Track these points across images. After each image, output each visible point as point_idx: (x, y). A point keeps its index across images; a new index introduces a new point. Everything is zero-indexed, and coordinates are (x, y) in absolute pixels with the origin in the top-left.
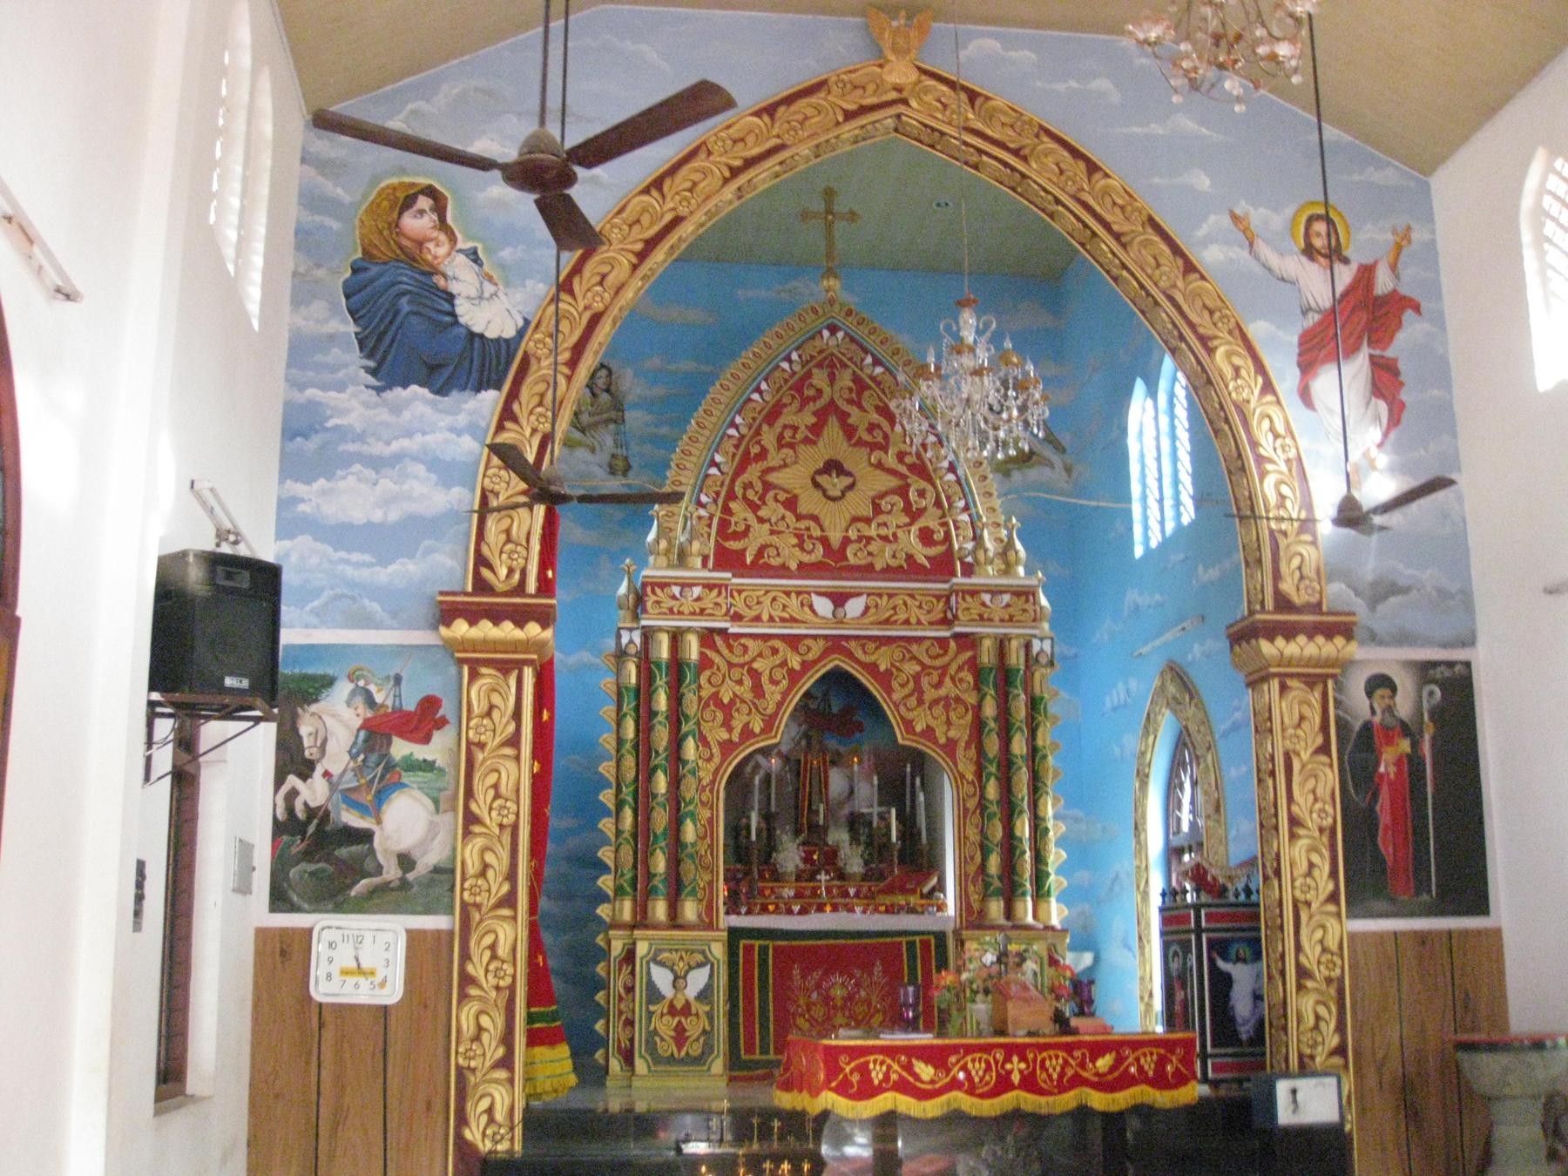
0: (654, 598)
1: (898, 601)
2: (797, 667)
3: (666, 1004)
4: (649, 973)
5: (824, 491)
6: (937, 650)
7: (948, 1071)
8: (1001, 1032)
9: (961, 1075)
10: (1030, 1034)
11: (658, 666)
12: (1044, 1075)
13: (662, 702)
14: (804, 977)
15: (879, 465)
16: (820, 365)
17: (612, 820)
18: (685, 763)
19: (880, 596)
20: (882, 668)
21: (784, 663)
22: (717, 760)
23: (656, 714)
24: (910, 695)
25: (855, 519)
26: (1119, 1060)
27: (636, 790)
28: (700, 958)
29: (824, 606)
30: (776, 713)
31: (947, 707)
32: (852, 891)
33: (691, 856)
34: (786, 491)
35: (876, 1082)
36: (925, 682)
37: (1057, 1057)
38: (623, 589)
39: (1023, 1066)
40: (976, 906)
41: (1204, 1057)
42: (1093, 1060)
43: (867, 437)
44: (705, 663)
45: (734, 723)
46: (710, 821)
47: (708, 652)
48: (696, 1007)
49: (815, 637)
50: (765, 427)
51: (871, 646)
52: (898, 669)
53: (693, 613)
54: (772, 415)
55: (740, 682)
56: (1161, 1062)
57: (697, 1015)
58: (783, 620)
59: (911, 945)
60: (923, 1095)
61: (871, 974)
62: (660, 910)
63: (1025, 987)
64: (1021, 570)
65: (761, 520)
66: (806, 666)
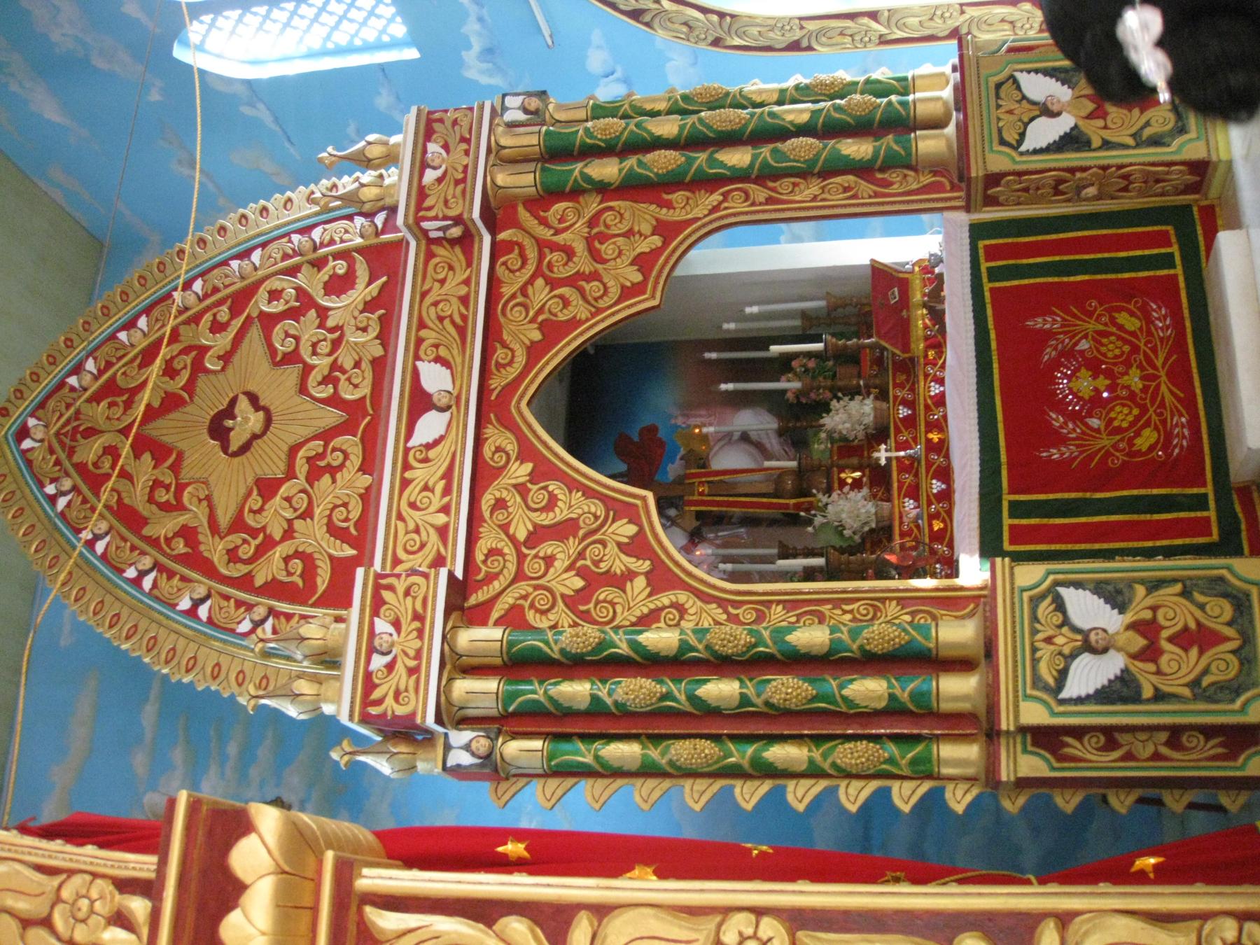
0: (390, 701)
1: (430, 315)
2: (528, 467)
3: (1138, 667)
4: (1079, 700)
5: (255, 437)
6: (513, 258)
11: (512, 696)
13: (576, 691)
14: (1061, 440)
15: (226, 358)
16: (71, 452)
17: (791, 785)
18: (684, 646)
19: (420, 341)
20: (536, 336)
21: (521, 489)
22: (683, 597)
23: (595, 699)
24: (582, 292)
25: (303, 389)
27: (733, 738)
28: (1045, 607)
29: (430, 426)
30: (604, 499)
31: (603, 238)
32: (903, 412)
33: (854, 634)
34: (249, 494)
36: (562, 272)
38: (383, 766)
40: (927, 179)
43: (185, 375)
44: (514, 619)
45: (618, 568)
46: (790, 605)
47: (495, 615)
48: (1140, 608)
49: (479, 442)
50: (147, 531)
51: (500, 354)
52: (540, 311)
53: (420, 632)
54: (129, 518)
55: (549, 560)
57: (1154, 609)
58: (447, 491)
59: (994, 274)
61: (1050, 334)
62: (957, 689)
64: (395, 139)
65: (289, 534)
66: (527, 452)
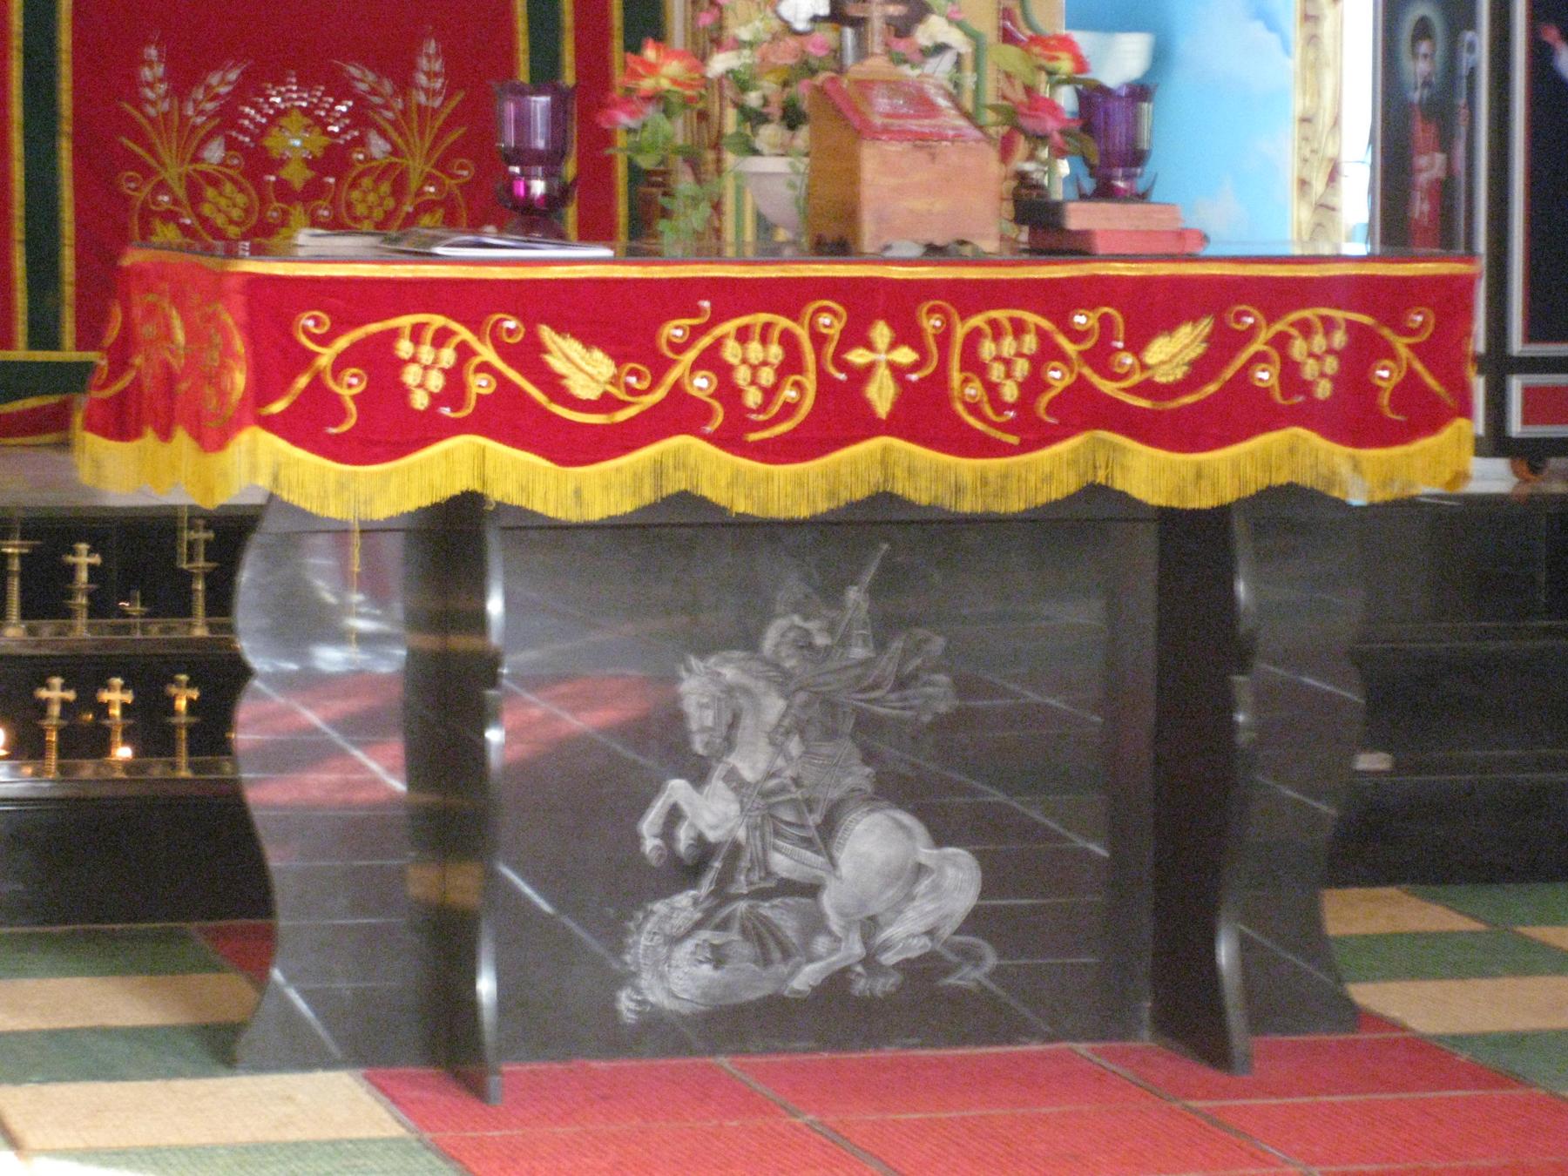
7: (660, 367)
8: (842, 248)
9: (702, 384)
10: (935, 253)
12: (975, 390)
26: (1224, 344)
35: (420, 401)
37: (1019, 328)
39: (905, 355)
41: (1499, 365)
42: (1137, 345)
56: (1363, 350)
60: (572, 446)
61: (405, 84)
63: (925, 106)
